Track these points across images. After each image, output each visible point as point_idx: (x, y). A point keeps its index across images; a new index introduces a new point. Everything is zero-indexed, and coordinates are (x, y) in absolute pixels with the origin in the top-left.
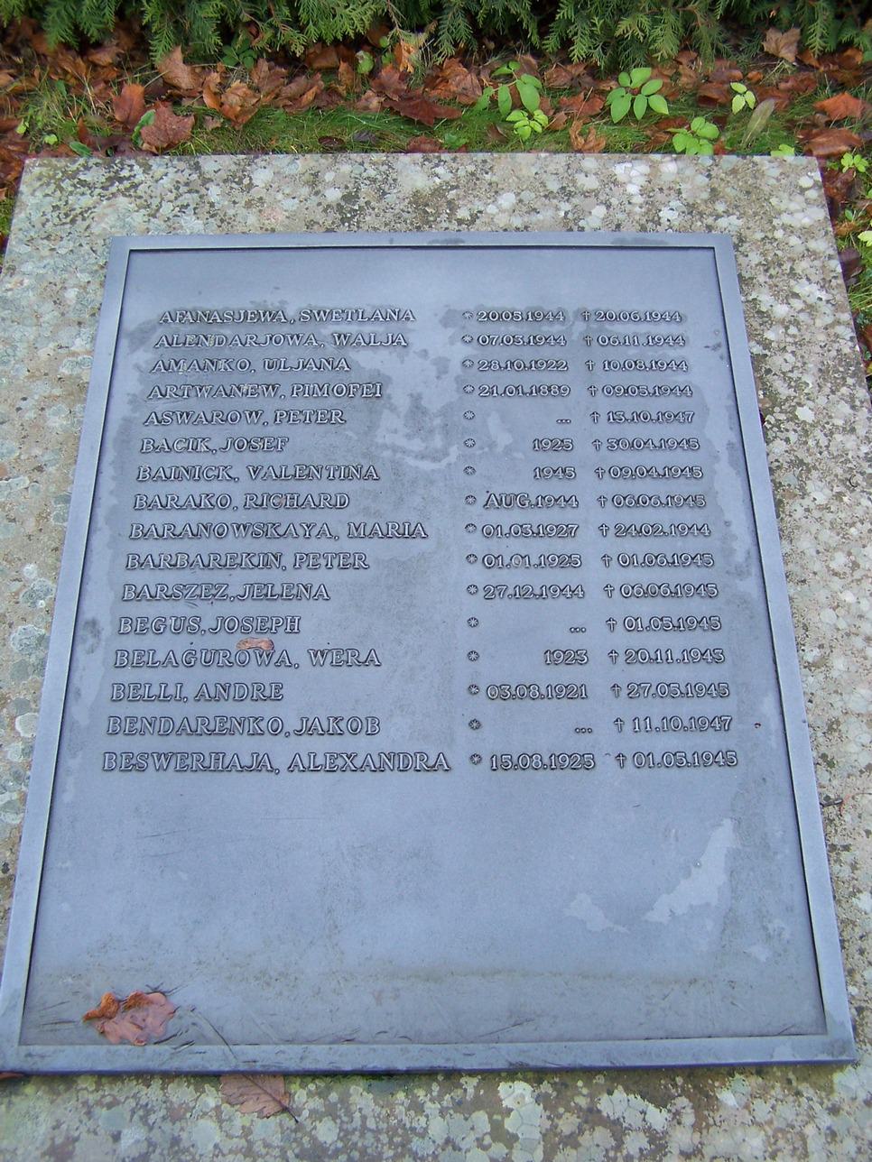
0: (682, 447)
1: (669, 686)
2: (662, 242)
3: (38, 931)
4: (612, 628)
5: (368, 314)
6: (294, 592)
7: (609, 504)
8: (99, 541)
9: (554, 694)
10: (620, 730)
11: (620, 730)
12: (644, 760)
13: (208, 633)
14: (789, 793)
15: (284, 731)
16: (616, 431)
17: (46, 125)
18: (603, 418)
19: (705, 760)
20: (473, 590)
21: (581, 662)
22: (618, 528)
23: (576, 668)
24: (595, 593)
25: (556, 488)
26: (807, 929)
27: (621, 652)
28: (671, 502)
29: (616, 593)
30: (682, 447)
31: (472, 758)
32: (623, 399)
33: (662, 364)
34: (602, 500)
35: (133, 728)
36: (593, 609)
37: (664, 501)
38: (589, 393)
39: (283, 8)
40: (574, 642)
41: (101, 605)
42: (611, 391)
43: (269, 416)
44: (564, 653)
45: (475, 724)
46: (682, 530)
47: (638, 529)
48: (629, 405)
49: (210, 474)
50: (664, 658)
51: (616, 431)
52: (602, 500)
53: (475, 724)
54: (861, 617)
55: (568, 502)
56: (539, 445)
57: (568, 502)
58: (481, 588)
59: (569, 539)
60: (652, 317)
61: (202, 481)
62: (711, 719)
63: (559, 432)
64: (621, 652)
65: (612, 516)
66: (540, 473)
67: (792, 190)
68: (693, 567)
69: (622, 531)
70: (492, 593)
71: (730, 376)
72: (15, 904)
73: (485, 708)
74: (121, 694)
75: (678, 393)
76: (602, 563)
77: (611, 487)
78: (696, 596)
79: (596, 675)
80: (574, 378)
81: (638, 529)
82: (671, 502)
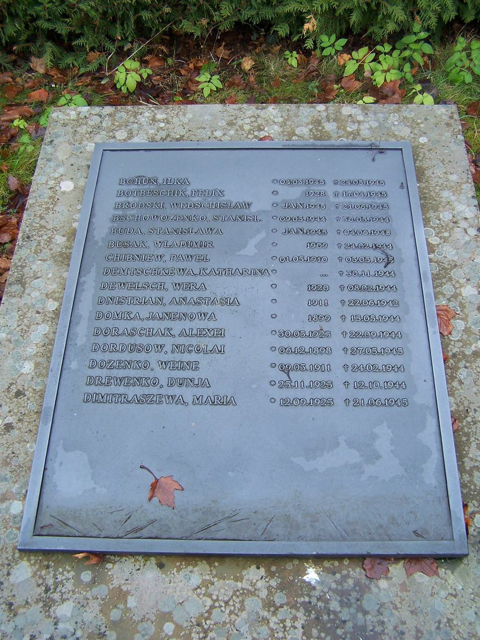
1: (371, 349)
3: (44, 490)
4: (339, 233)
5: (233, 205)
7: (346, 289)
13: (145, 320)
17: (38, 352)
18: (349, 318)
20: (274, 349)
22: (351, 333)
23: (325, 339)
24: (338, 385)
25: (317, 252)
28: (382, 335)
31: (273, 182)
32: (356, 264)
40: (322, 281)
43: (168, 348)
44: (320, 400)
45: (273, 365)
46: (388, 368)
47: (364, 367)
48: (362, 311)
49: (142, 332)
52: (342, 288)
55: (324, 245)
56: (311, 288)
57: (324, 245)
58: (277, 382)
60: (368, 183)
64: (349, 349)
65: (349, 296)
66: (311, 318)
73: (280, 188)
74: (114, 231)
77: (349, 296)
78: (389, 321)
79: (339, 393)
82: (382, 335)
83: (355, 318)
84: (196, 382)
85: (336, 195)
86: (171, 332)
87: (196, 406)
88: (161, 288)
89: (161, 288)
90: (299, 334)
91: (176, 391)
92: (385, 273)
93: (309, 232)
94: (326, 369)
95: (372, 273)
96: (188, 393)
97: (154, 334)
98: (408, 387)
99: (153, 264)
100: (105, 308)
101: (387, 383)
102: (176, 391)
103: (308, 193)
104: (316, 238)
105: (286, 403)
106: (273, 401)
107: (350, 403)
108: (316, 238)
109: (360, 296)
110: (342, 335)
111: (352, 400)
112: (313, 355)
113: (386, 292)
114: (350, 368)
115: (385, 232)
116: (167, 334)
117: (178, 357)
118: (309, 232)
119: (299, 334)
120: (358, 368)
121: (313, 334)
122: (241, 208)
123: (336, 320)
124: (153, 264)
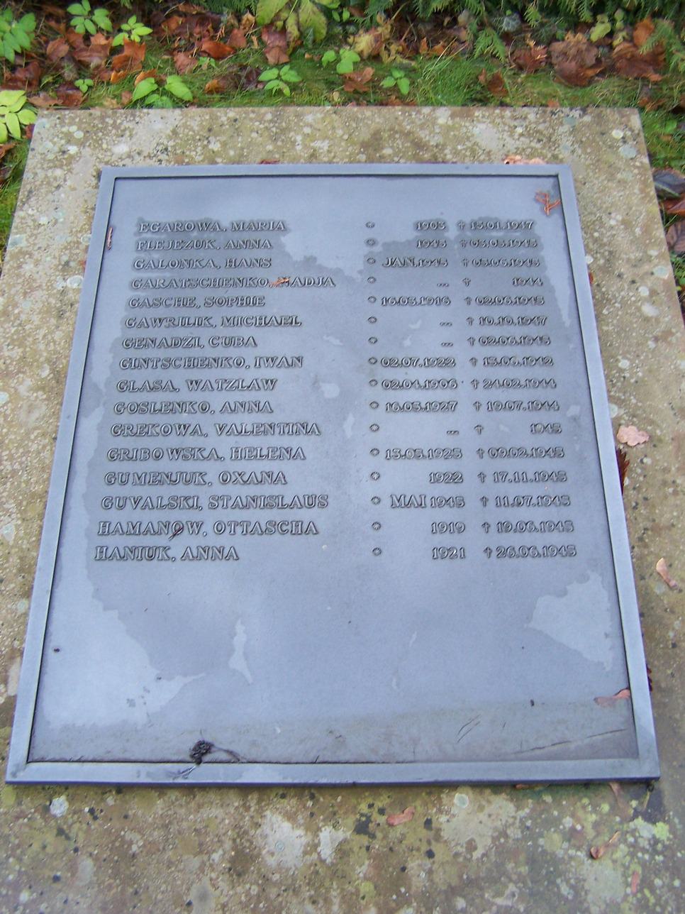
8: (79, 486)
10: (485, 505)
11: (485, 505)
12: (503, 553)
14: (591, 429)
19: (549, 551)
26: (624, 662)
27: (494, 549)
29: (485, 455)
34: (475, 383)
35: (142, 344)
36: (464, 418)
37: (541, 552)
39: (215, 81)
41: (103, 371)
46: (549, 526)
50: (521, 478)
59: (450, 413)
61: (144, 560)
63: (445, 353)
65: (482, 373)
67: (626, 132)
69: (489, 385)
73: (378, 463)
75: (547, 407)
78: (546, 457)
80: (464, 395)
81: (501, 383)
83: (489, 362)
84: (174, 478)
86: (205, 478)
87: (131, 536)
88: (260, 324)
89: (260, 324)
90: (521, 453)
91: (198, 397)
93: (514, 263)
94: (503, 504)
95: (530, 476)
97: (108, 556)
103: (421, 225)
104: (524, 272)
107: (492, 554)
108: (524, 272)
109: (498, 352)
115: (535, 300)
116: (184, 505)
117: (189, 293)
118: (514, 263)
119: (521, 453)
121: (537, 453)
122: (256, 230)
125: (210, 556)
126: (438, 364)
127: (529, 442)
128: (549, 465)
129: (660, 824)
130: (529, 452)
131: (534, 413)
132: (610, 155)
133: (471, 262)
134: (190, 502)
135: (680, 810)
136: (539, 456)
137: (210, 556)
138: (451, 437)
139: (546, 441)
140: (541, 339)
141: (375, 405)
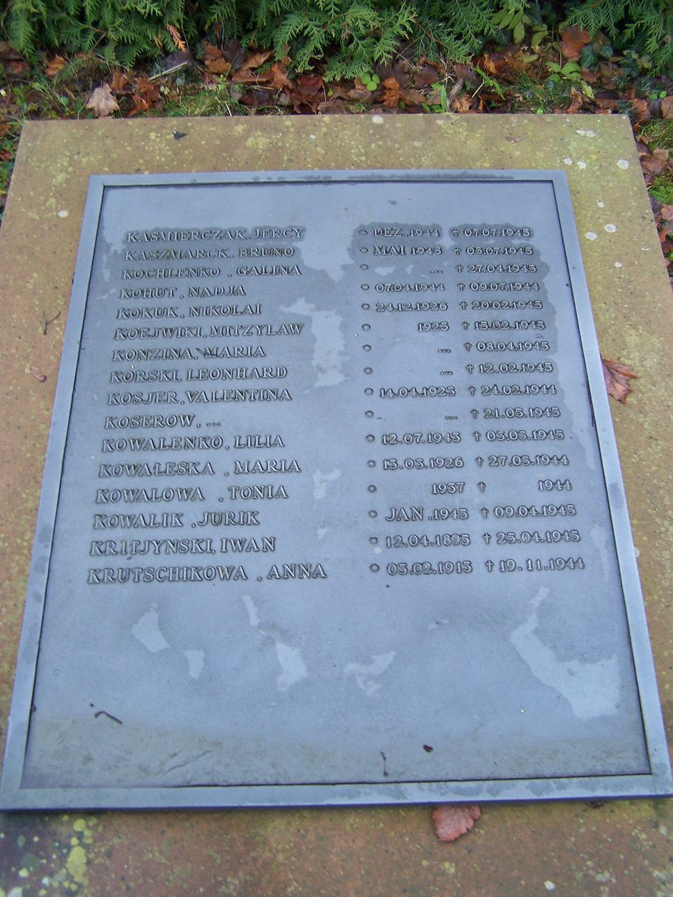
0: (546, 415)
2: (510, 177)
3: (38, 680)
6: (233, 396)
9: (436, 465)
15: (225, 444)
16: (489, 380)
21: (464, 543)
30: (546, 415)
33: (528, 345)
34: (487, 537)
38: (460, 307)
42: (483, 348)
45: (372, 488)
48: (496, 359)
51: (489, 380)
53: (372, 489)
54: (669, 406)
62: (544, 410)
68: (562, 541)
70: (391, 466)
71: (574, 320)
72: (16, 696)
73: (375, 402)
74: (100, 548)
75: (556, 461)
76: (466, 371)
78: (540, 393)
85: (464, 305)
91: (234, 559)
92: (536, 367)
95: (545, 563)
96: (256, 564)
98: (586, 566)
99: (179, 431)
100: (110, 509)
101: (540, 457)
102: (234, 559)
105: (396, 570)
106: (372, 463)
110: (485, 568)
111: (469, 303)
112: (443, 547)
113: (554, 491)
114: (486, 462)
115: (536, 323)
116: (196, 549)
120: (490, 390)
123: (471, 490)
124: (179, 431)
125: (197, 445)
126: (430, 308)
127: (540, 499)
128: (561, 524)
129: (668, 551)
130: (523, 389)
131: (546, 493)
132: (592, 151)
133: (474, 346)
134: (203, 546)
135: (667, 347)
136: (553, 541)
137: (197, 445)
138: (445, 376)
139: (557, 498)
140: (534, 303)
141: (366, 306)
